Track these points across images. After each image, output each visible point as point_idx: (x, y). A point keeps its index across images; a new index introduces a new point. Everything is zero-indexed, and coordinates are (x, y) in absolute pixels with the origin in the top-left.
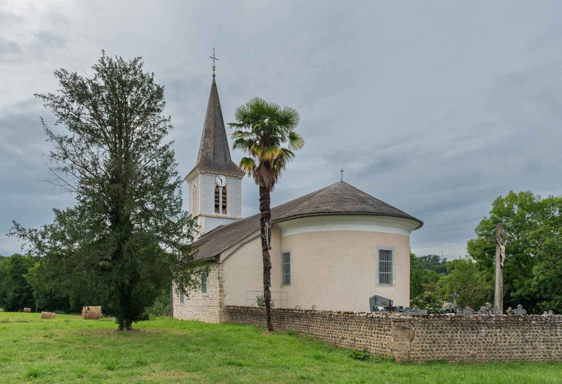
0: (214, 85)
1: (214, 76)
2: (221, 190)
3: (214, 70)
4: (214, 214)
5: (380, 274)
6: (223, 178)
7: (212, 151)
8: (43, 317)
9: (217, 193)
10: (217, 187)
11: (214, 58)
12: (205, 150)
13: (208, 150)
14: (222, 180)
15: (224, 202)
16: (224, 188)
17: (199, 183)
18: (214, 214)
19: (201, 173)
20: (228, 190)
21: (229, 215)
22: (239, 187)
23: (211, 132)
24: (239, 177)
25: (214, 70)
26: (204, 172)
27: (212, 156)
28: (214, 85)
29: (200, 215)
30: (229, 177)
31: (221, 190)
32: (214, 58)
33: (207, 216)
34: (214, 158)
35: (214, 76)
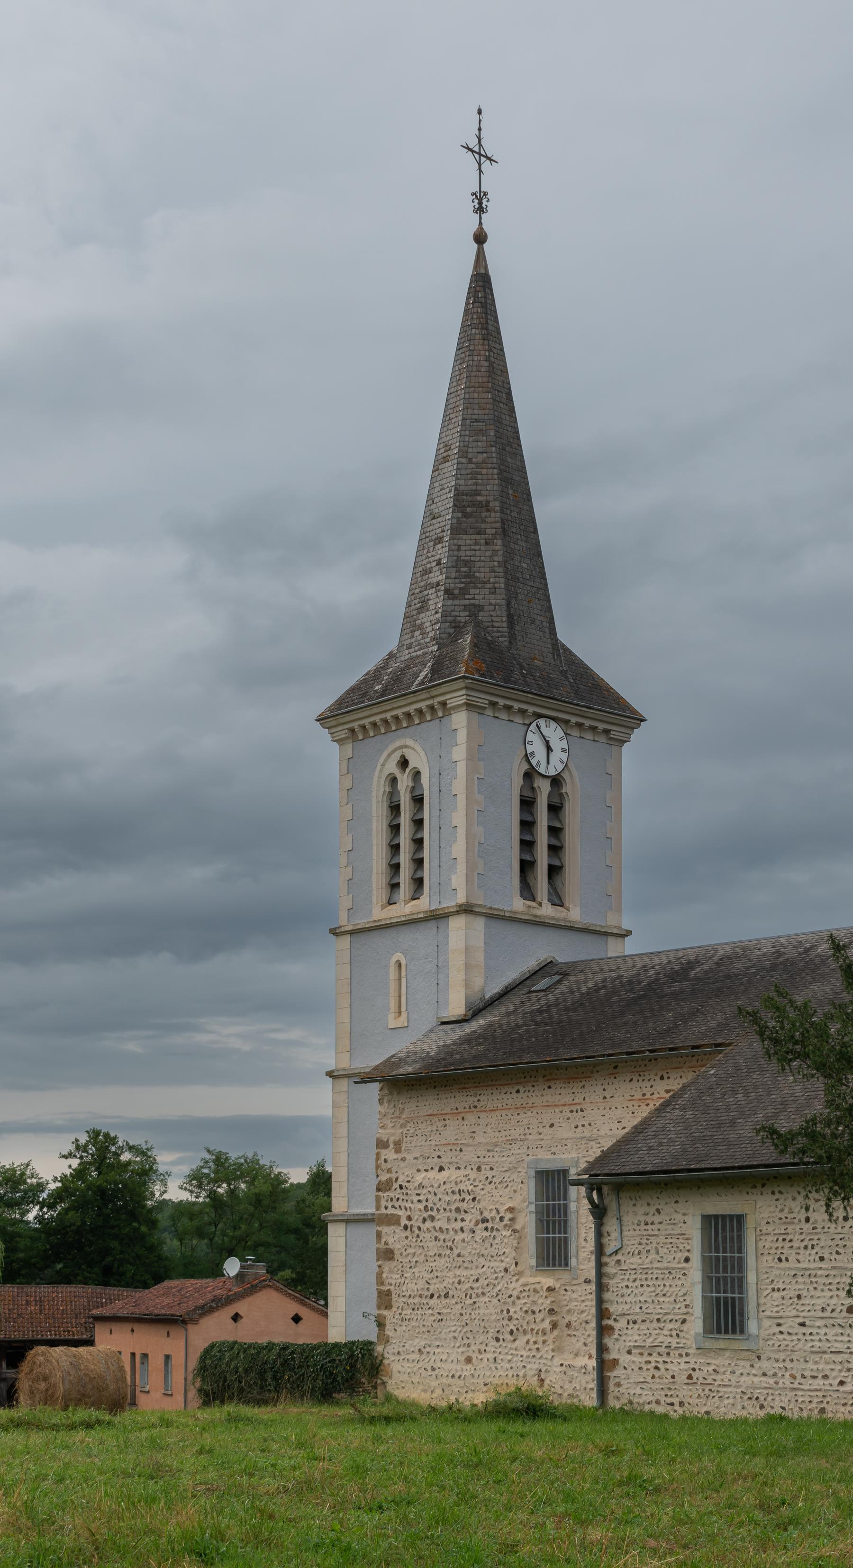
0: (481, 285)
1: (480, 238)
2: (544, 788)
3: (480, 210)
4: (518, 905)
5: (565, 1233)
6: (554, 732)
7: (500, 599)
8: (233, 1419)
9: (527, 803)
10: (530, 775)
11: (480, 155)
12: (464, 592)
13: (479, 596)
14: (550, 746)
15: (555, 850)
16: (556, 781)
17: (459, 753)
18: (518, 905)
19: (469, 706)
20: (572, 789)
21: (575, 914)
22: (612, 778)
23: (487, 507)
24: (617, 732)
25: (480, 210)
26: (482, 699)
27: (502, 623)
28: (481, 285)
29: (466, 909)
30: (575, 733)
31: (544, 788)
32: (480, 155)
33: (494, 916)
34: (512, 637)
35: (480, 238)
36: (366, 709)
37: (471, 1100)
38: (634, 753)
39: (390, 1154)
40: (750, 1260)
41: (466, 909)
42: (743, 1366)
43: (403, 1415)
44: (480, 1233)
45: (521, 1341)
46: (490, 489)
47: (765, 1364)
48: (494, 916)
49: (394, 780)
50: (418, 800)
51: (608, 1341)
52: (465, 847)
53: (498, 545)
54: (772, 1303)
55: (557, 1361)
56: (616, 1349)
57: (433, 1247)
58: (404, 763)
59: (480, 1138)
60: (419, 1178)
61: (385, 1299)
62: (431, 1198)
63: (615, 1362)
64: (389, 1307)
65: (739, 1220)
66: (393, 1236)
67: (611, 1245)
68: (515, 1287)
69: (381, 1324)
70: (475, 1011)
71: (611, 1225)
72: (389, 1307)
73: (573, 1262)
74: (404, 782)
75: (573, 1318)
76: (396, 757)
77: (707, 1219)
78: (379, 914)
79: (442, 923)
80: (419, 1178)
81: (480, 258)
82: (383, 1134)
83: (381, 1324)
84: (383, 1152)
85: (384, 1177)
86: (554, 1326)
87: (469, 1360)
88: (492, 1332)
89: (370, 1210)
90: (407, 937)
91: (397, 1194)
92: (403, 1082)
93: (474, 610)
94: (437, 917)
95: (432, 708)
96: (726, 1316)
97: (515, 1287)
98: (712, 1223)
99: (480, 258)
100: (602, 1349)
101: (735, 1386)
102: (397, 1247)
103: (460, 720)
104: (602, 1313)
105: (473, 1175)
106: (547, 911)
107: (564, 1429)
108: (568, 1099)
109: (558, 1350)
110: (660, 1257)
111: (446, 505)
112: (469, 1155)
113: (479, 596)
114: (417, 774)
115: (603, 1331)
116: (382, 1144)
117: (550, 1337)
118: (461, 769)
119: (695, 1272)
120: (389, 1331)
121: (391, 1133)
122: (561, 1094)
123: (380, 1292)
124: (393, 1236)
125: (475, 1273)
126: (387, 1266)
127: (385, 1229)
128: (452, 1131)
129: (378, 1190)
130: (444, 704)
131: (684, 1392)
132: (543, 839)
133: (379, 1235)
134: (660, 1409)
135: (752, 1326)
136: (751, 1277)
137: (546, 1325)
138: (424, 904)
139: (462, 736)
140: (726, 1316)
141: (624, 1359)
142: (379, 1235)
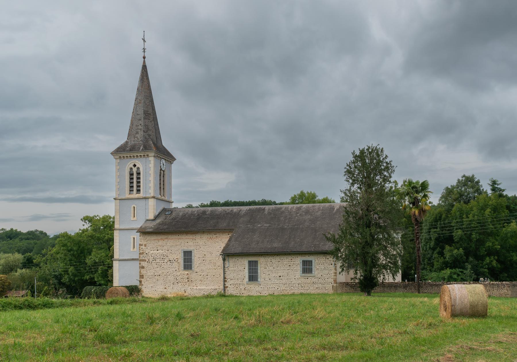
1: (144, 58)
4: (160, 196)
10: (161, 169)
12: (147, 131)
18: (160, 196)
28: (144, 67)
29: (154, 197)
33: (157, 199)
35: (144, 58)
36: (121, 152)
37: (166, 237)
38: (174, 166)
39: (143, 247)
40: (259, 268)
41: (154, 197)
42: (257, 287)
43: (145, 300)
44: (169, 263)
45: (180, 284)
46: (150, 111)
47: (261, 286)
48: (157, 199)
49: (131, 169)
50: (139, 174)
51: (226, 283)
52: (149, 184)
53: (153, 123)
54: (263, 276)
55: (189, 288)
56: (227, 284)
57: (156, 266)
58: (135, 166)
59: (168, 244)
60: (152, 252)
61: (142, 276)
62: (155, 256)
63: (227, 287)
64: (143, 278)
65: (311, 262)
66: (143, 264)
67: (226, 266)
68: (178, 274)
69: (140, 282)
70: (156, 217)
71: (227, 262)
72: (143, 278)
73: (193, 269)
74: (135, 170)
75: (193, 279)
76: (133, 164)
77: (249, 261)
78: (128, 196)
79: (147, 200)
80: (152, 252)
81: (144, 62)
82: (141, 243)
83: (140, 282)
84: (141, 247)
85: (141, 252)
86: (188, 281)
87: (166, 288)
88: (172, 283)
89: (138, 257)
90: (137, 202)
91: (146, 255)
92: (144, 232)
93: (149, 135)
94: (145, 198)
95: (144, 155)
96: (253, 277)
97: (178, 274)
98: (304, 263)
99: (144, 62)
100: (224, 284)
101: (254, 290)
102: (145, 266)
103: (152, 159)
104: (225, 278)
105: (167, 252)
106: (163, 197)
107: (230, 299)
108: (192, 237)
109: (189, 286)
110: (240, 268)
111: (141, 112)
112: (165, 248)
113: (150, 133)
114: (138, 168)
115: (225, 281)
116: (140, 245)
117: (187, 283)
118: (152, 169)
119: (247, 271)
120: (143, 283)
121: (143, 242)
122: (191, 236)
123: (140, 276)
124: (143, 264)
125: (168, 271)
126: (142, 270)
127: (142, 262)
128: (161, 243)
129: (140, 254)
130: (148, 155)
131: (243, 292)
132: (135, 180)
133: (140, 264)
134: (238, 295)
135: (259, 280)
136: (259, 271)
137: (187, 281)
138: (141, 195)
139: (152, 162)
140: (253, 277)
141: (229, 286)
142: (140, 264)
